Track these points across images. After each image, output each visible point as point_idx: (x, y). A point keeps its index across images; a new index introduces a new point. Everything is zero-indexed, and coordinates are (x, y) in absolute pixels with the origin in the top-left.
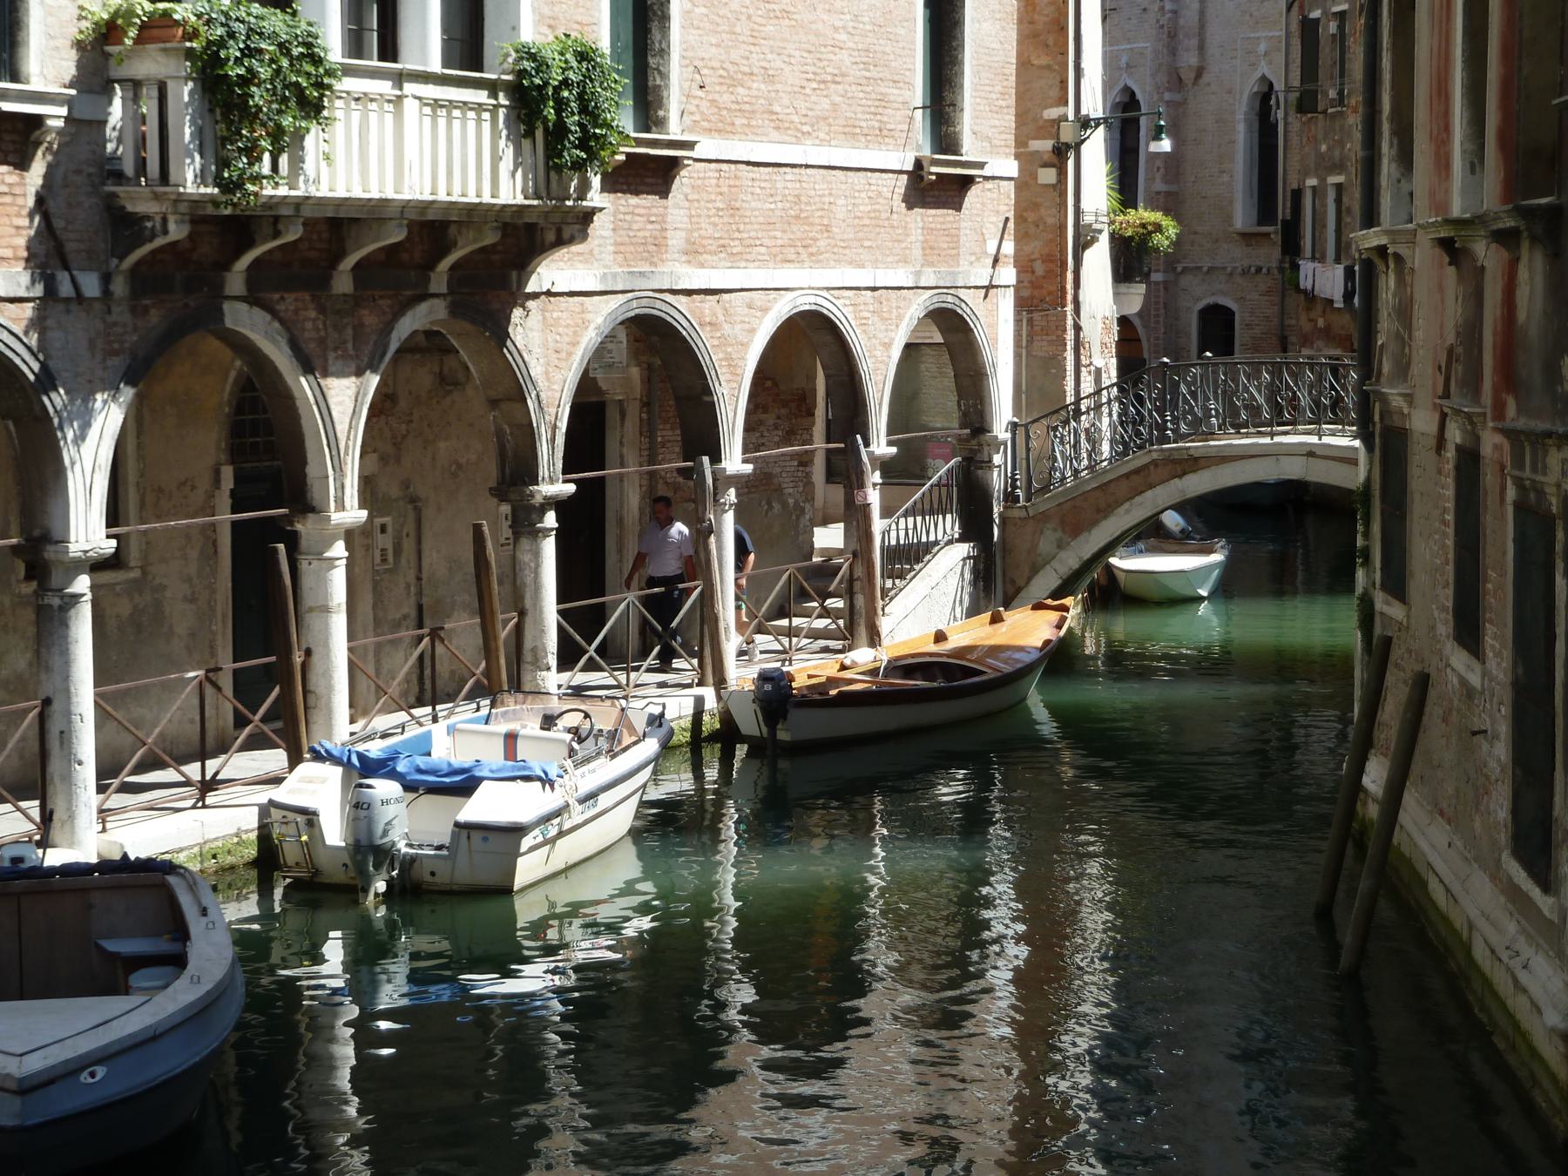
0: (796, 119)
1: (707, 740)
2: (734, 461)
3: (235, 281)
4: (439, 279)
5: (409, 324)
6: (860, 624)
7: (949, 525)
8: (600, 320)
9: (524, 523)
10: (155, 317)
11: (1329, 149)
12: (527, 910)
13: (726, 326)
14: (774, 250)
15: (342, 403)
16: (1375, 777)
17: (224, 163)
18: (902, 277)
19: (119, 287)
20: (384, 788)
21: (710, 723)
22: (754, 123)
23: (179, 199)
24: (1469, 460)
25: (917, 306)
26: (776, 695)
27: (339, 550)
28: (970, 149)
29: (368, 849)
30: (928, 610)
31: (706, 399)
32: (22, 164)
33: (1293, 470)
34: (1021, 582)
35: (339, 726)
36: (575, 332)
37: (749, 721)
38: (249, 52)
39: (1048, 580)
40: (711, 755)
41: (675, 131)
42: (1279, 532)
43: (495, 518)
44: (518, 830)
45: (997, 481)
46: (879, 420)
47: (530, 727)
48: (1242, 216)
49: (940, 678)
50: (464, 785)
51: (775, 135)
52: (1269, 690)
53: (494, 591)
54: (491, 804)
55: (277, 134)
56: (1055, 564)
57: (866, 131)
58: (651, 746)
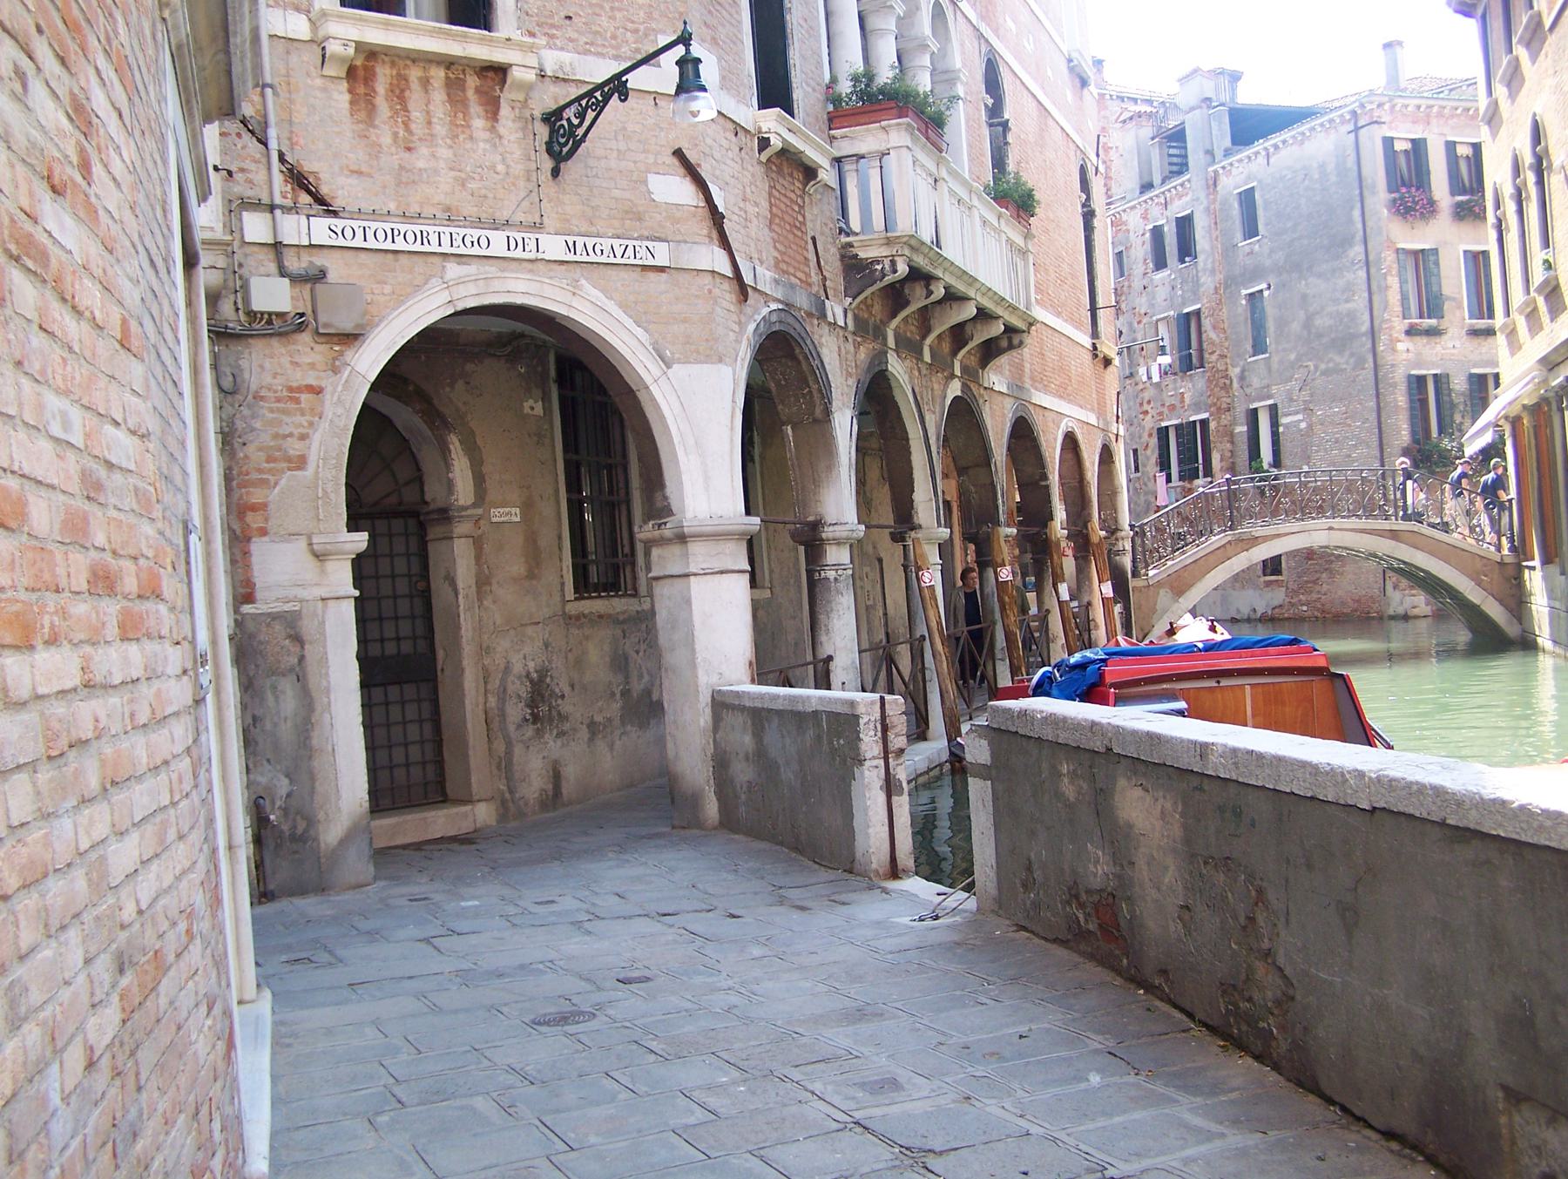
18: (1093, 421)
45: (1127, 561)
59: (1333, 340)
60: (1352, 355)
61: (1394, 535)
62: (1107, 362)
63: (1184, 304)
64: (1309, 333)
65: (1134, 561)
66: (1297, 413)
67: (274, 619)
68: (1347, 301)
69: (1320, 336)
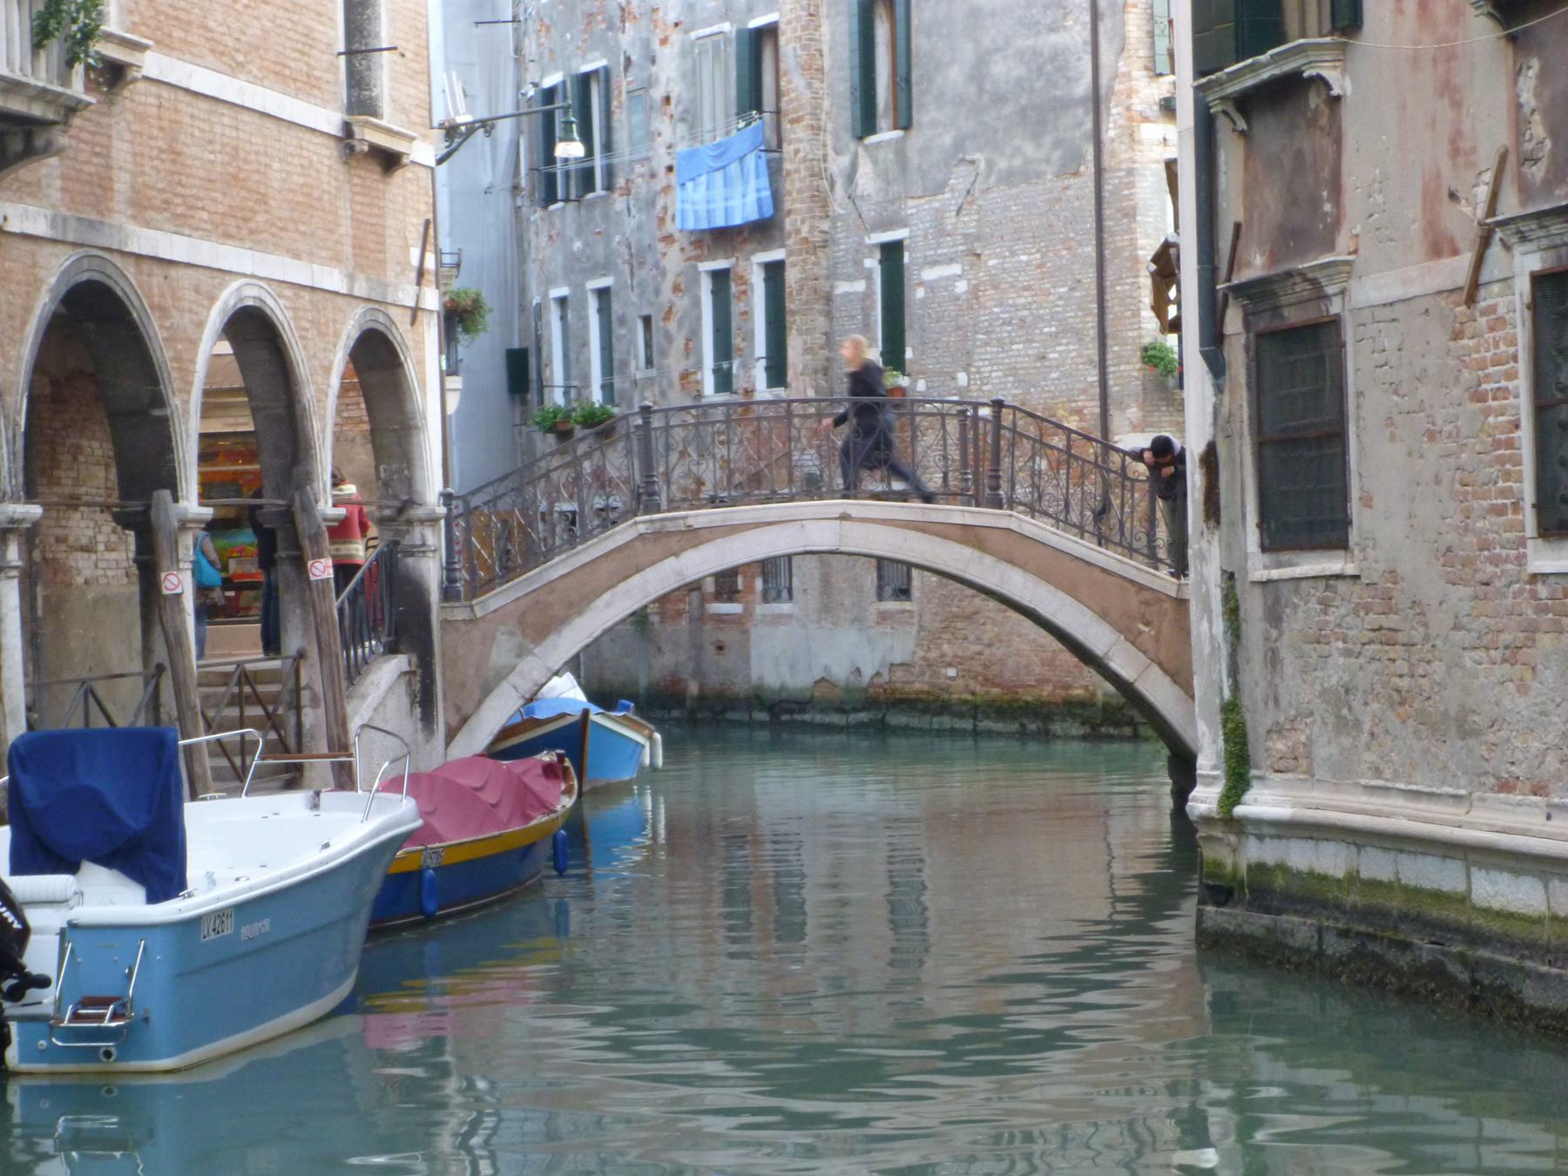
0: (230, 42)
8: (53, 280)
11: (587, 244)
13: (175, 314)
14: (217, 218)
18: (333, 279)
22: (190, 39)
31: (157, 412)
34: (468, 707)
36: (28, 293)
45: (431, 571)
51: (210, 59)
56: (513, 678)
57: (295, 75)
59: (1023, 111)
60: (1057, 144)
61: (970, 536)
62: (389, 161)
63: (751, 11)
64: (981, 90)
65: (449, 568)
66: (951, 261)
67: (490, 581)
68: (1052, 29)
69: (999, 99)
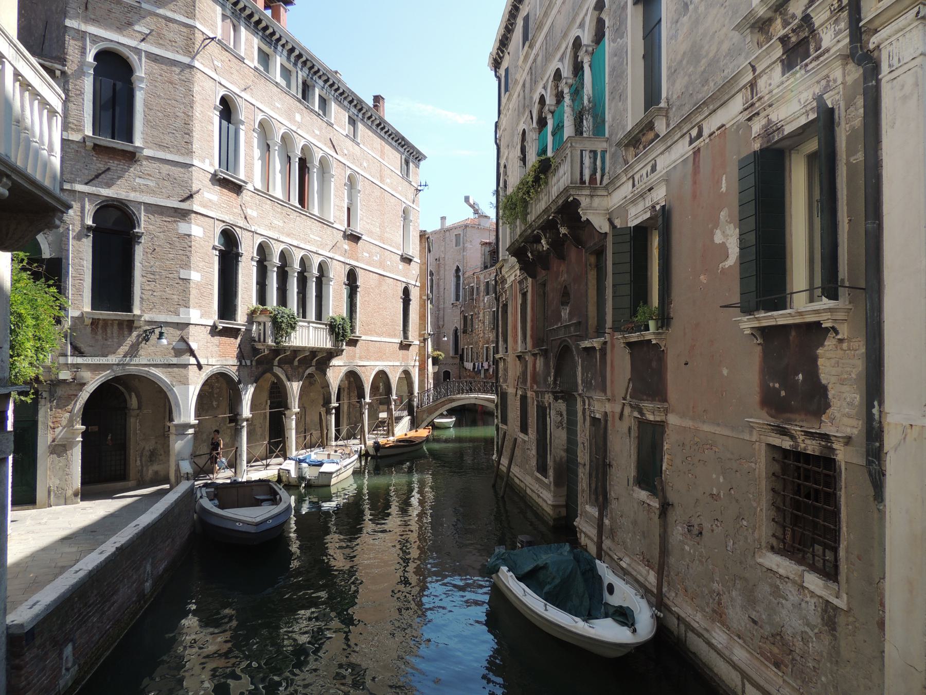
1: (363, 456)
2: (368, 400)
3: (276, 363)
4: (314, 363)
5: (308, 372)
6: (390, 432)
7: (406, 413)
9: (328, 412)
10: (260, 369)
12: (333, 490)
15: (295, 388)
16: (504, 461)
17: (276, 339)
18: (398, 364)
19: (254, 363)
20: (304, 465)
21: (363, 452)
23: (268, 346)
24: (524, 398)
25: (401, 369)
26: (377, 446)
27: (294, 417)
28: (411, 339)
29: (301, 478)
30: (402, 430)
32: (236, 338)
33: (473, 401)
35: (294, 453)
37: (372, 452)
38: (282, 317)
39: (425, 423)
40: (363, 459)
41: (357, 334)
42: (467, 415)
43: (323, 410)
44: (331, 473)
45: (415, 404)
46: (394, 392)
47: (333, 453)
48: (451, 353)
49: (407, 443)
50: (320, 464)
52: (457, 445)
53: (322, 425)
54: (326, 468)
55: (287, 333)
58: (356, 456)
